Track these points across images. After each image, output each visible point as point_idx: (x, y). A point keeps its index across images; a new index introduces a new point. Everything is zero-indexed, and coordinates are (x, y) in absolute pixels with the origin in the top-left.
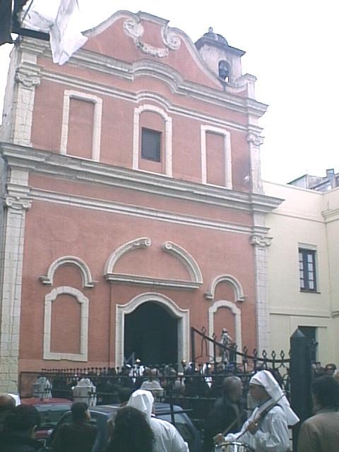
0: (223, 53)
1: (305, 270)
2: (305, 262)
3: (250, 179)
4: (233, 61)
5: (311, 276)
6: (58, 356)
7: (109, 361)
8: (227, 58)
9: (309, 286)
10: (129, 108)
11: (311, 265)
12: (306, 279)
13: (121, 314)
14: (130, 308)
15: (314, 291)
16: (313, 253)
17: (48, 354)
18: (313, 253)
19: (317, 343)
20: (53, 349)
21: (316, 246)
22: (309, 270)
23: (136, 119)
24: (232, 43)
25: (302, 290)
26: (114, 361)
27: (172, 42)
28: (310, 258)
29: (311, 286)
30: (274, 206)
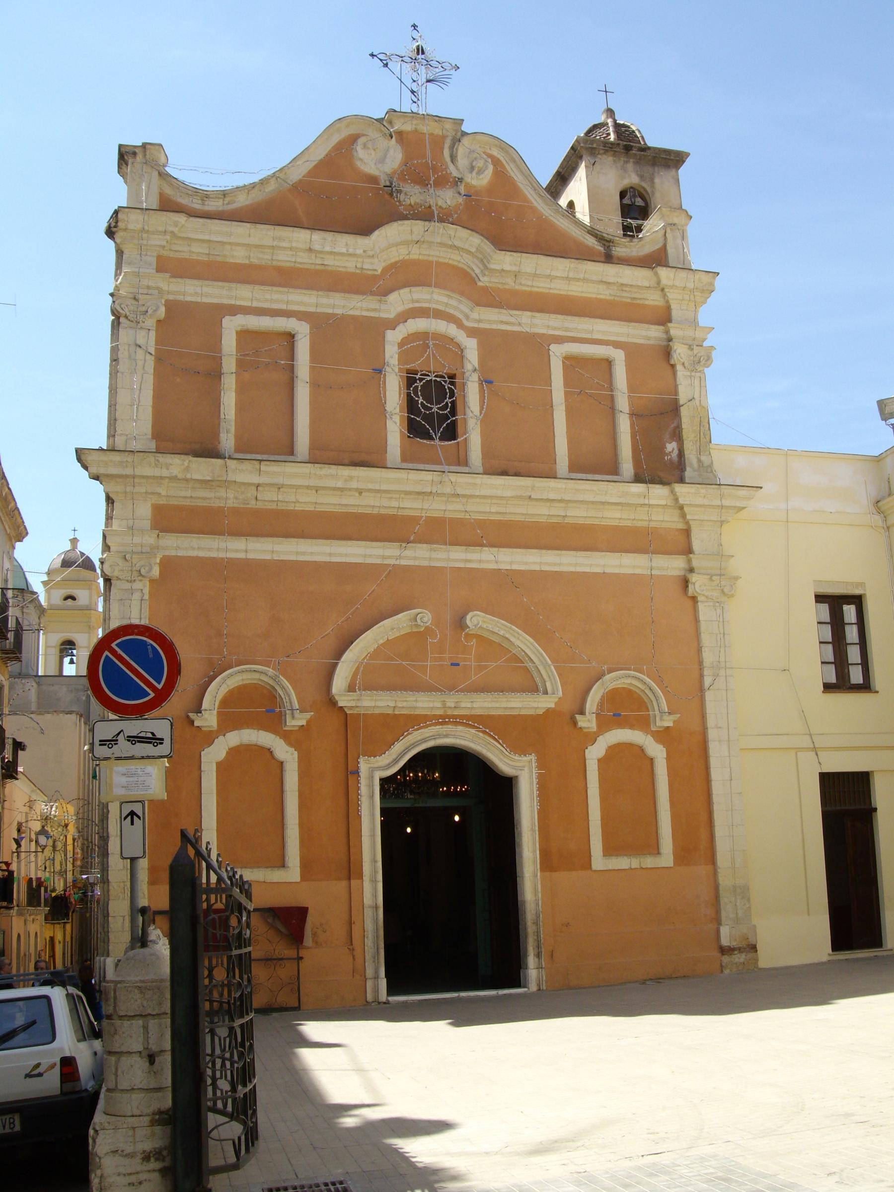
0: (630, 166)
1: (838, 641)
2: (837, 623)
3: (681, 454)
4: (657, 180)
5: (854, 654)
6: (622, 863)
7: (349, 879)
8: (642, 177)
9: (847, 673)
10: (373, 330)
11: (855, 629)
12: (840, 662)
13: (372, 777)
14: (390, 761)
15: (866, 687)
16: (858, 601)
17: (599, 861)
18: (858, 601)
19: (875, 810)
20: (610, 850)
21: (862, 584)
22: (849, 640)
23: (392, 354)
24: (654, 139)
25: (828, 687)
26: (361, 877)
27: (472, 168)
28: (849, 612)
29: (856, 676)
30: (739, 504)
